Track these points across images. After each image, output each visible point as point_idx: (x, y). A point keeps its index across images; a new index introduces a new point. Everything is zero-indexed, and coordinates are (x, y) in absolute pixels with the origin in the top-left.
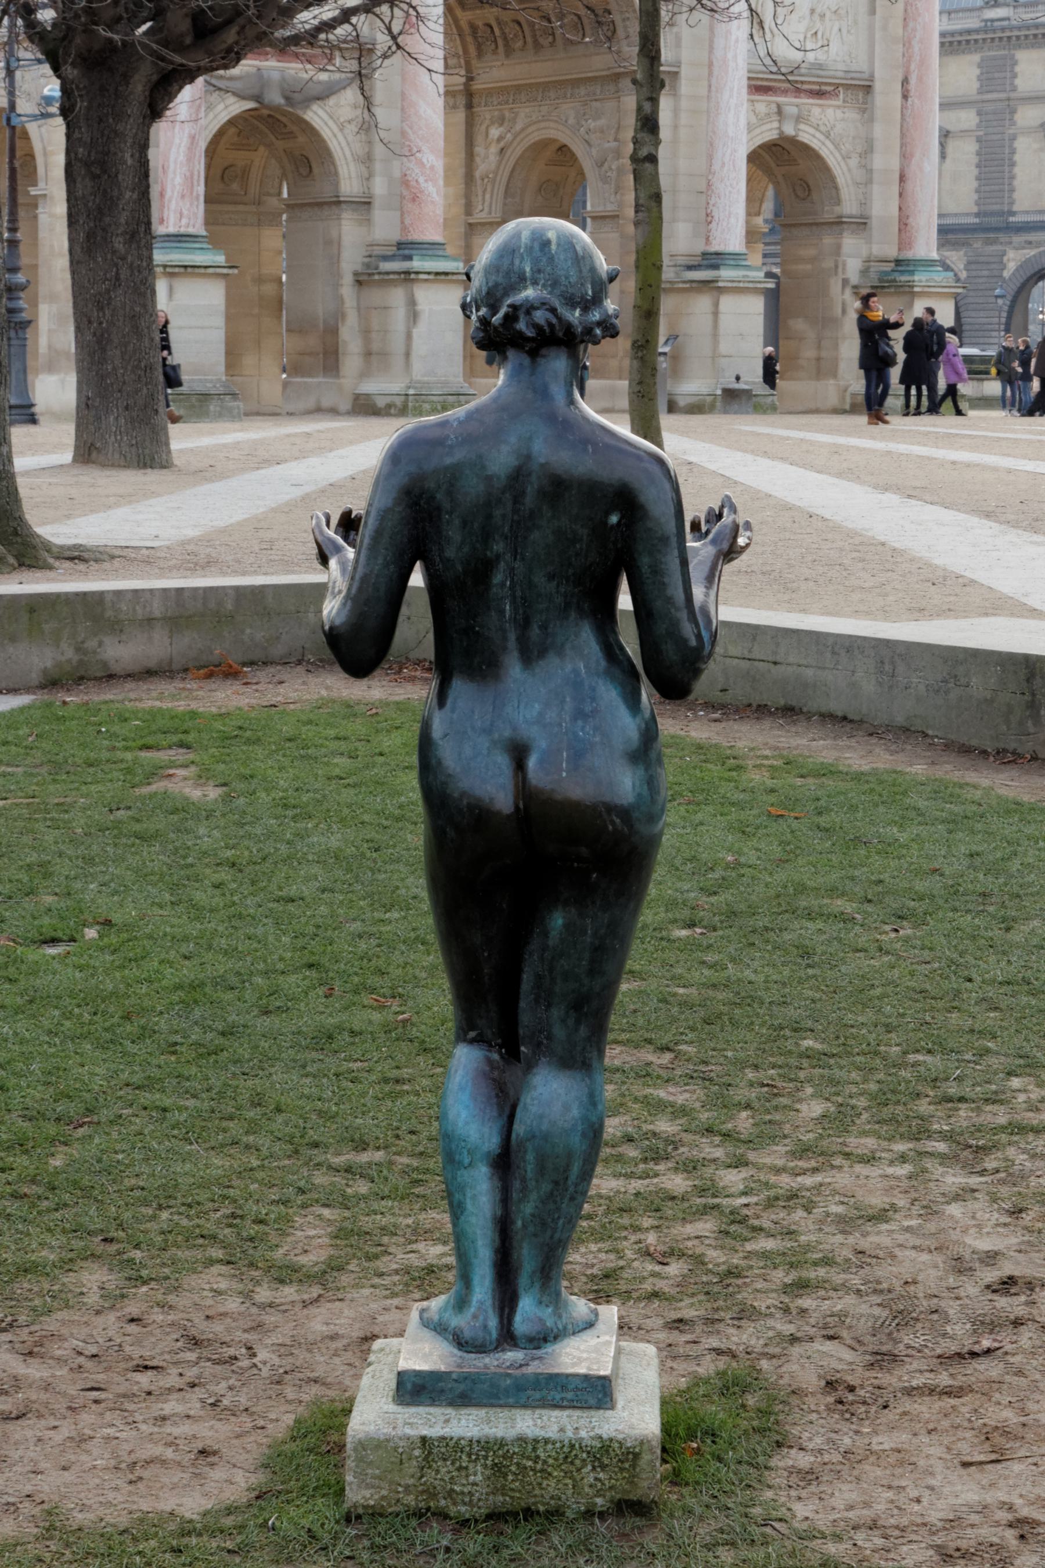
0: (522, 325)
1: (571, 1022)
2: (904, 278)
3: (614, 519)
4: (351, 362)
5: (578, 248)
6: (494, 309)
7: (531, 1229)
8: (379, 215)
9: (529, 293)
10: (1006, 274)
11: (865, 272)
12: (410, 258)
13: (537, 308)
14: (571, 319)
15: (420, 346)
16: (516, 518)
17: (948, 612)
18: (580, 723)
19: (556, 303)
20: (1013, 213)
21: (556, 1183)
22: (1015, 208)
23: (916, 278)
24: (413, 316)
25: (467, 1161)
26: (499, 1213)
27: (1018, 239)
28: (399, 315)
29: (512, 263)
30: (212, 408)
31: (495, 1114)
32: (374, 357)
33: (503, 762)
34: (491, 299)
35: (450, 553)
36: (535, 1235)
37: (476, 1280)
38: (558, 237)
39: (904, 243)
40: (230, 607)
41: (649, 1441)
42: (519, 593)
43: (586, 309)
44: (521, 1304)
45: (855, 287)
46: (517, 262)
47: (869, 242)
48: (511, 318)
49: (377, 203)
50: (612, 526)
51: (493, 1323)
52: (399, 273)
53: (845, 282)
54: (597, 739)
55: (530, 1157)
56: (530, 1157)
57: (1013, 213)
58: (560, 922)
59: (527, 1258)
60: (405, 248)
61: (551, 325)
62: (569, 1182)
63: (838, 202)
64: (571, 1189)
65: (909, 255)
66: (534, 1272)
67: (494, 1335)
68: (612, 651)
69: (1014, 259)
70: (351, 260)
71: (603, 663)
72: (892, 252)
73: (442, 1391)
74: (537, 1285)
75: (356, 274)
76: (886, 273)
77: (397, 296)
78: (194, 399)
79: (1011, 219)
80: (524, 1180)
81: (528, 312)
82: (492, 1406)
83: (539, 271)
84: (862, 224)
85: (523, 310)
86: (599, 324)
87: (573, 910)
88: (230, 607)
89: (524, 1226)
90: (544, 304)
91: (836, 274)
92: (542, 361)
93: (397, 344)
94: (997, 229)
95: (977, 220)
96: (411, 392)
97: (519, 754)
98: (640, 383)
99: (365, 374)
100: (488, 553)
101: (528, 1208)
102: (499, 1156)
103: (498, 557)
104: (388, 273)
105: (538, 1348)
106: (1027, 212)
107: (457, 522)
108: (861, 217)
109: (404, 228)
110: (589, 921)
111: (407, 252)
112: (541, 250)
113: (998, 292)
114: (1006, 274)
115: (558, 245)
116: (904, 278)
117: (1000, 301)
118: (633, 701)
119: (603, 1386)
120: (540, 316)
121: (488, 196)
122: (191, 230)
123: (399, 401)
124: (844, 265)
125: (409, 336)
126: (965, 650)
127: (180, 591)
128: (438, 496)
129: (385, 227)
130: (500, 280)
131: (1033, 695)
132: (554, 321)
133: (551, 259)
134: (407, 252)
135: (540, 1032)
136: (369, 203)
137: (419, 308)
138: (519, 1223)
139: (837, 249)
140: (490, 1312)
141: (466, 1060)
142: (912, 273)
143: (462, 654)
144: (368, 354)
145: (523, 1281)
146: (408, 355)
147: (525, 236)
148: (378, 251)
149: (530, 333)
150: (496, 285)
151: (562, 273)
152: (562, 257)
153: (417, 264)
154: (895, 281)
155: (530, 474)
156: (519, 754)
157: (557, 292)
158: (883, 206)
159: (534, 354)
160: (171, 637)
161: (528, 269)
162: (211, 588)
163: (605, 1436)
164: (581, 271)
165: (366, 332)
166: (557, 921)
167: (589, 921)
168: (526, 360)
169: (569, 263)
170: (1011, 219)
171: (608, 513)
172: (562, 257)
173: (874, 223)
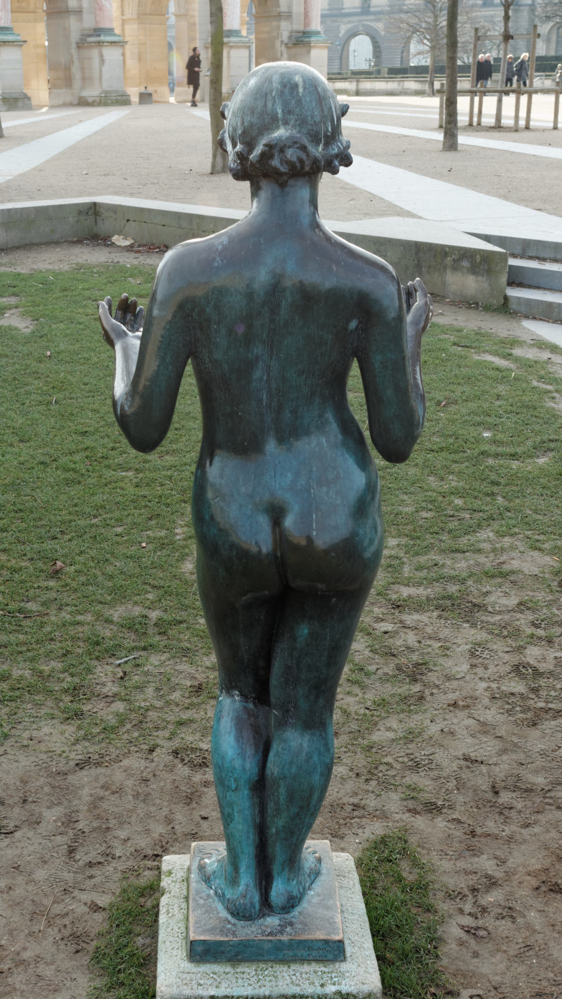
0: (276, 162)
1: (312, 697)
2: (307, 40)
3: (353, 325)
4: (77, 83)
5: (319, 89)
6: (250, 145)
7: (283, 835)
8: (85, 16)
9: (281, 133)
10: (340, 35)
11: (290, 37)
12: (99, 36)
13: (290, 147)
14: (317, 154)
15: (105, 76)
16: (272, 326)
17: (367, 215)
18: (325, 489)
19: (305, 141)
20: (343, 9)
21: (302, 808)
22: (345, 6)
23: (312, 39)
24: (102, 61)
25: (234, 786)
26: (258, 821)
27: (345, 20)
28: (96, 61)
29: (265, 106)
30: (20, 104)
31: (253, 752)
32: (86, 80)
33: (264, 522)
34: (248, 139)
35: (218, 355)
36: (286, 839)
37: (243, 869)
38: (304, 81)
39: (307, 24)
40: (33, 217)
41: (375, 994)
42: (274, 386)
43: (327, 144)
44: (275, 884)
45: (286, 44)
46: (270, 104)
47: (292, 24)
48: (266, 156)
49: (84, 11)
50: (351, 331)
51: (257, 898)
52: (95, 43)
53: (282, 42)
54: (339, 501)
55: (283, 790)
56: (283, 790)
57: (343, 9)
58: (306, 631)
59: (279, 853)
60: (98, 31)
61: (301, 161)
62: (311, 805)
63: (278, 6)
64: (312, 809)
65: (308, 29)
66: (284, 862)
67: (257, 906)
68: (348, 426)
69: (344, 29)
70: (75, 37)
71: (340, 437)
72: (301, 28)
73: (223, 952)
74: (287, 869)
75: (77, 43)
76: (299, 37)
77: (95, 53)
78: (12, 101)
79: (343, 11)
80: (277, 803)
81: (282, 151)
82: (259, 961)
83: (290, 112)
84: (289, 16)
85: (278, 148)
86: (337, 156)
87: (316, 623)
88: (33, 217)
89: (277, 833)
90: (295, 143)
91: (278, 38)
92: (287, 189)
93: (96, 75)
94: (336, 16)
95: (328, 12)
96: (103, 95)
97: (276, 513)
98: (214, 100)
99: (83, 88)
100: (250, 356)
101: (280, 822)
102: (257, 782)
103: (257, 358)
104: (91, 43)
105: (288, 912)
106: (349, 8)
107: (223, 331)
108: (289, 12)
109: (97, 22)
110: (328, 630)
111: (98, 33)
112: (291, 93)
113: (337, 43)
114: (340, 35)
115: (305, 88)
116: (307, 40)
117: (339, 47)
118: (364, 462)
119: (338, 947)
120: (291, 154)
121: (131, 6)
122: (6, 25)
123: (98, 99)
124: (281, 34)
125: (101, 71)
126: (385, 239)
127: (9, 210)
128: (208, 310)
129: (88, 22)
130: (255, 120)
131: (419, 261)
132: (304, 157)
133: (299, 102)
134: (98, 33)
135: (288, 703)
136: (81, 11)
137: (105, 58)
138: (274, 830)
139: (278, 28)
140: (255, 891)
141: (230, 705)
142: (310, 37)
143: (231, 432)
144: (84, 79)
145: (276, 868)
146: (100, 79)
147: (276, 79)
148: (86, 32)
149: (283, 169)
150: (251, 125)
151: (309, 113)
152: (308, 99)
153: (102, 38)
154: (303, 41)
155: (284, 290)
156: (276, 513)
157: (304, 131)
158: (298, 9)
159: (283, 185)
160: (6, 232)
161: (279, 111)
162: (24, 208)
163: (344, 992)
164: (323, 110)
165: (83, 69)
166: (304, 631)
167: (328, 630)
168: (277, 190)
169: (314, 104)
170: (343, 11)
171: (348, 321)
172: (308, 99)
173: (294, 16)
